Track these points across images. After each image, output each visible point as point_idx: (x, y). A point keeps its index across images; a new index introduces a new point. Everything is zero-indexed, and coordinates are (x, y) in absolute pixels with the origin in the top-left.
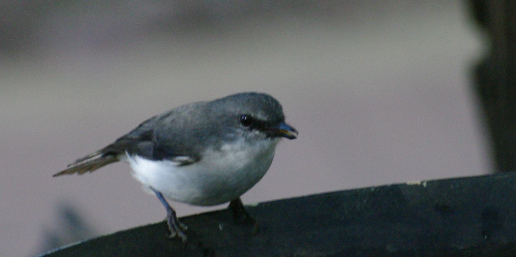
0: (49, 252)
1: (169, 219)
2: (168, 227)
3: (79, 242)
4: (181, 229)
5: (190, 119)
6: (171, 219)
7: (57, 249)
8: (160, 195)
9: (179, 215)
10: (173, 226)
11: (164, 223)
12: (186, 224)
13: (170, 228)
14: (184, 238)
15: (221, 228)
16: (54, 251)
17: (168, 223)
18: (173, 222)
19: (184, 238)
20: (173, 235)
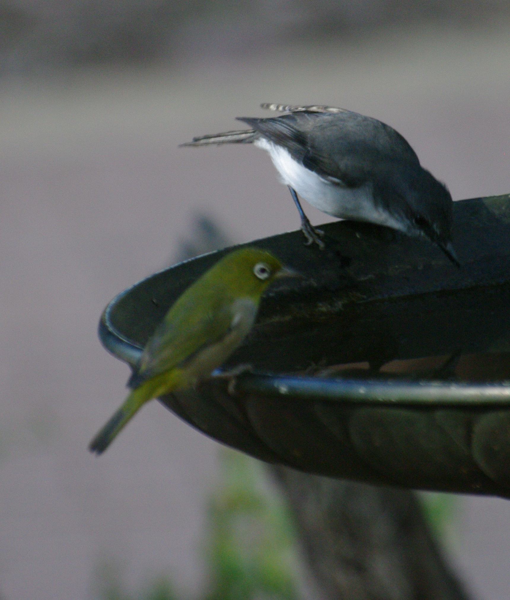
0: (185, 262)
1: (303, 228)
2: (303, 234)
3: (215, 251)
4: (318, 235)
5: (298, 120)
6: (306, 225)
7: (193, 258)
8: (295, 194)
9: (314, 223)
10: (309, 233)
11: (300, 232)
12: (322, 230)
13: (306, 235)
14: (322, 245)
15: (358, 236)
16: (190, 260)
17: (304, 231)
18: (309, 230)
19: (322, 245)
20: (310, 241)
